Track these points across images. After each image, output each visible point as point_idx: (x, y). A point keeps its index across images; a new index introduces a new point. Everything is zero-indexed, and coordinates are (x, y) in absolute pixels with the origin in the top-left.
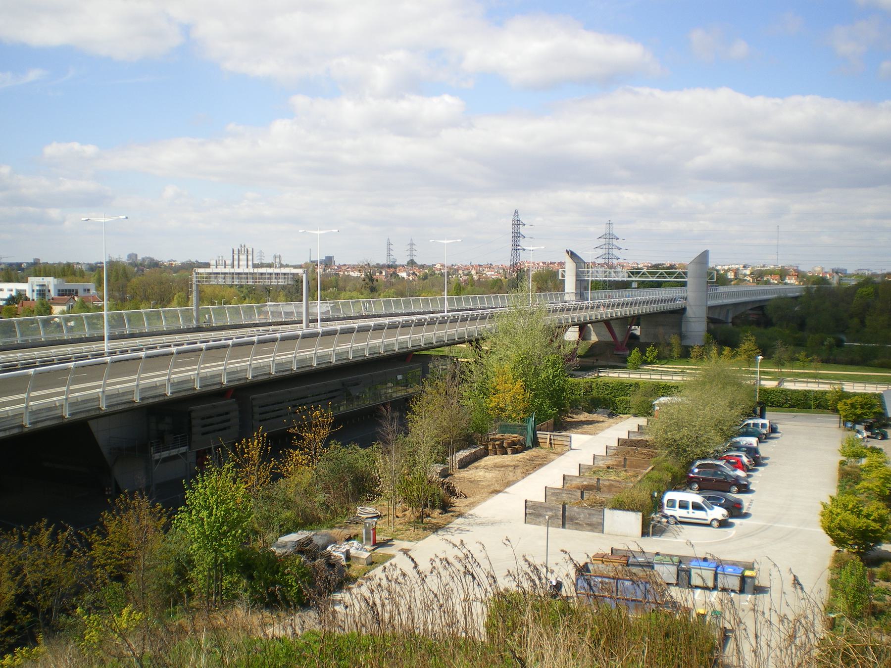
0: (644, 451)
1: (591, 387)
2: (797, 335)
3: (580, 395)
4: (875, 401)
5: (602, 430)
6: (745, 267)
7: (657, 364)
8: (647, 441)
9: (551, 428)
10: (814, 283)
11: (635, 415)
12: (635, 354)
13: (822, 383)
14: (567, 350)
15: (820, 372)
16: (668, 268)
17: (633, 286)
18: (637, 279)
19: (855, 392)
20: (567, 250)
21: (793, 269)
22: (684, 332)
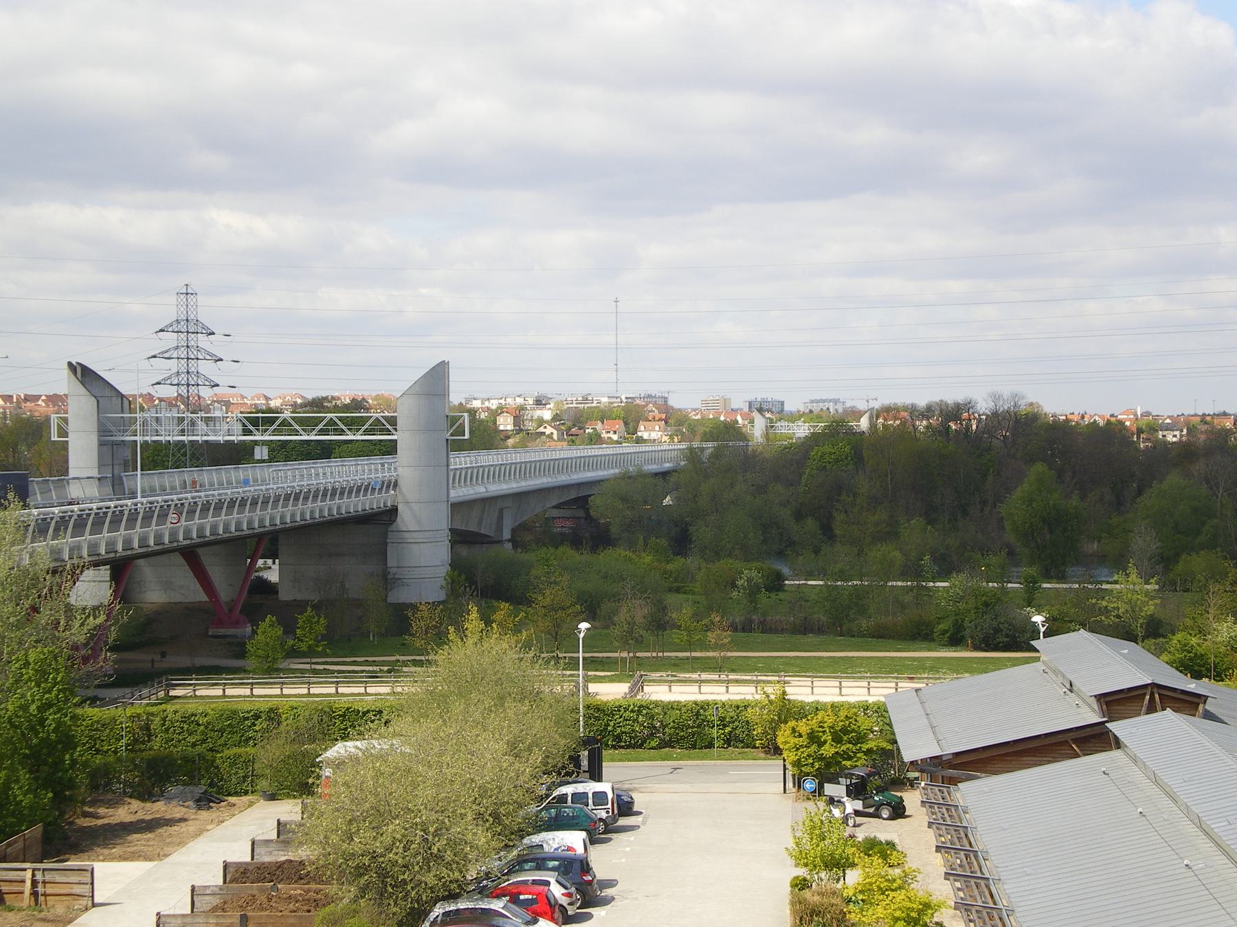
0: (296, 890)
1: (148, 729)
2: (670, 567)
3: (115, 752)
4: (864, 723)
5: (182, 843)
6: (539, 402)
7: (325, 655)
8: (302, 863)
9: (36, 850)
10: (707, 437)
11: (273, 797)
12: (267, 631)
13: (737, 681)
14: (78, 634)
15: (729, 654)
16: (346, 408)
17: (257, 456)
18: (267, 438)
19: (818, 702)
20: (70, 364)
21: (655, 404)
22: (393, 570)
